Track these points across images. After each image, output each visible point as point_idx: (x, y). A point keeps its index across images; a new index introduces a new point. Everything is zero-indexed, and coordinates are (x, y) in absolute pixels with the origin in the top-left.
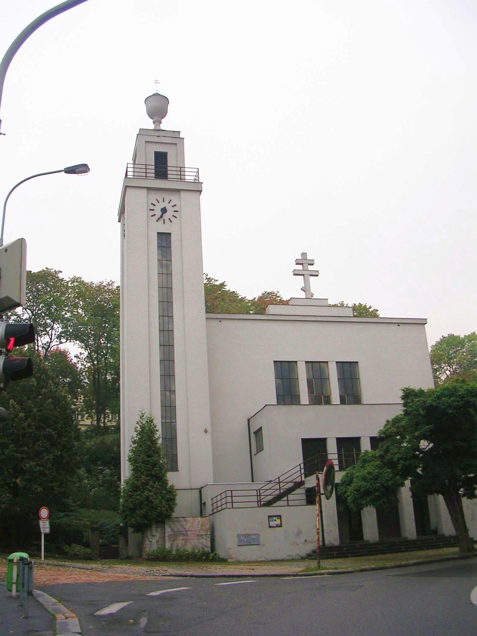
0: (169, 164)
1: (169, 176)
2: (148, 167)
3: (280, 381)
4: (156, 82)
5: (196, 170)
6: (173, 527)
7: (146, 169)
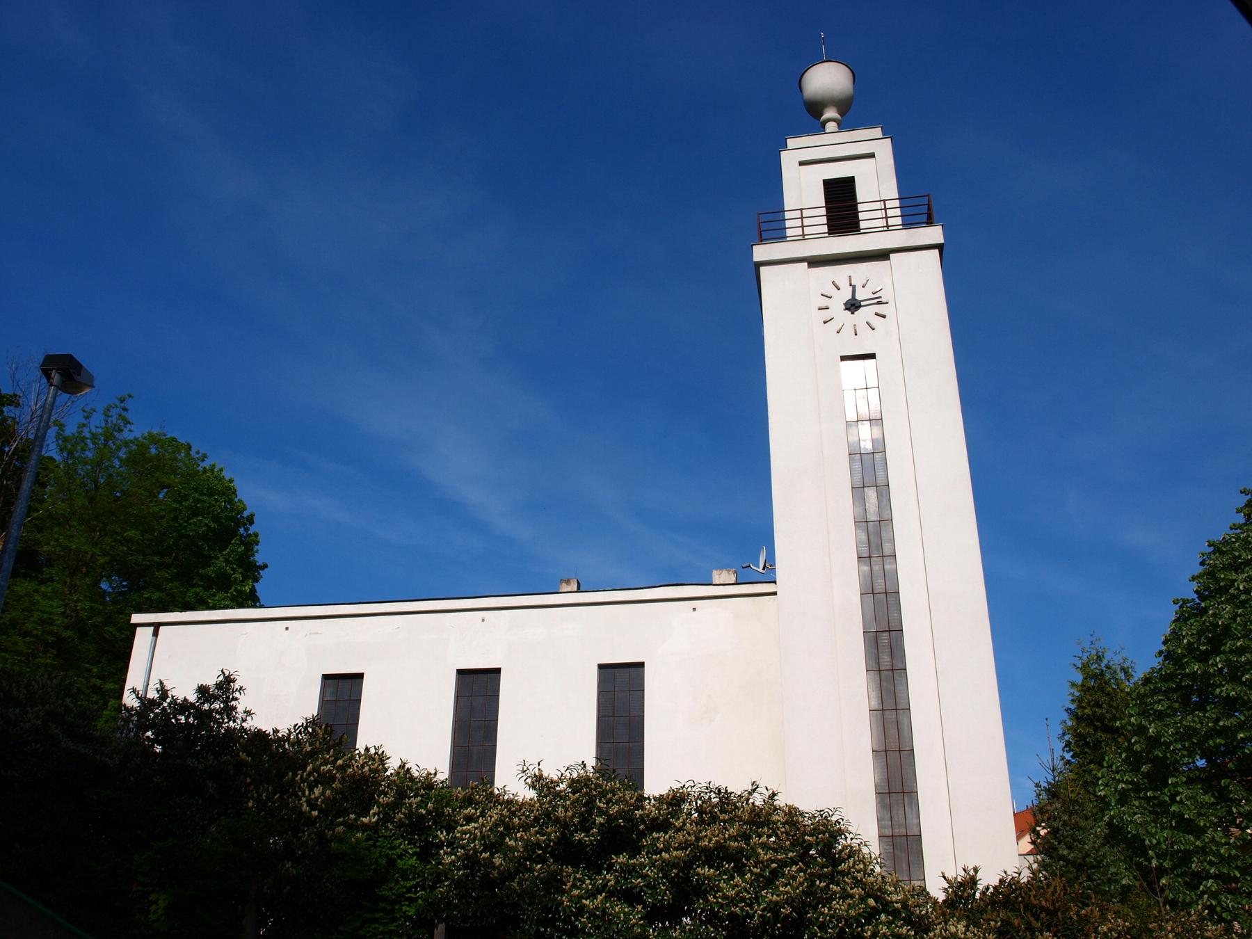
0: (860, 197)
1: (862, 225)
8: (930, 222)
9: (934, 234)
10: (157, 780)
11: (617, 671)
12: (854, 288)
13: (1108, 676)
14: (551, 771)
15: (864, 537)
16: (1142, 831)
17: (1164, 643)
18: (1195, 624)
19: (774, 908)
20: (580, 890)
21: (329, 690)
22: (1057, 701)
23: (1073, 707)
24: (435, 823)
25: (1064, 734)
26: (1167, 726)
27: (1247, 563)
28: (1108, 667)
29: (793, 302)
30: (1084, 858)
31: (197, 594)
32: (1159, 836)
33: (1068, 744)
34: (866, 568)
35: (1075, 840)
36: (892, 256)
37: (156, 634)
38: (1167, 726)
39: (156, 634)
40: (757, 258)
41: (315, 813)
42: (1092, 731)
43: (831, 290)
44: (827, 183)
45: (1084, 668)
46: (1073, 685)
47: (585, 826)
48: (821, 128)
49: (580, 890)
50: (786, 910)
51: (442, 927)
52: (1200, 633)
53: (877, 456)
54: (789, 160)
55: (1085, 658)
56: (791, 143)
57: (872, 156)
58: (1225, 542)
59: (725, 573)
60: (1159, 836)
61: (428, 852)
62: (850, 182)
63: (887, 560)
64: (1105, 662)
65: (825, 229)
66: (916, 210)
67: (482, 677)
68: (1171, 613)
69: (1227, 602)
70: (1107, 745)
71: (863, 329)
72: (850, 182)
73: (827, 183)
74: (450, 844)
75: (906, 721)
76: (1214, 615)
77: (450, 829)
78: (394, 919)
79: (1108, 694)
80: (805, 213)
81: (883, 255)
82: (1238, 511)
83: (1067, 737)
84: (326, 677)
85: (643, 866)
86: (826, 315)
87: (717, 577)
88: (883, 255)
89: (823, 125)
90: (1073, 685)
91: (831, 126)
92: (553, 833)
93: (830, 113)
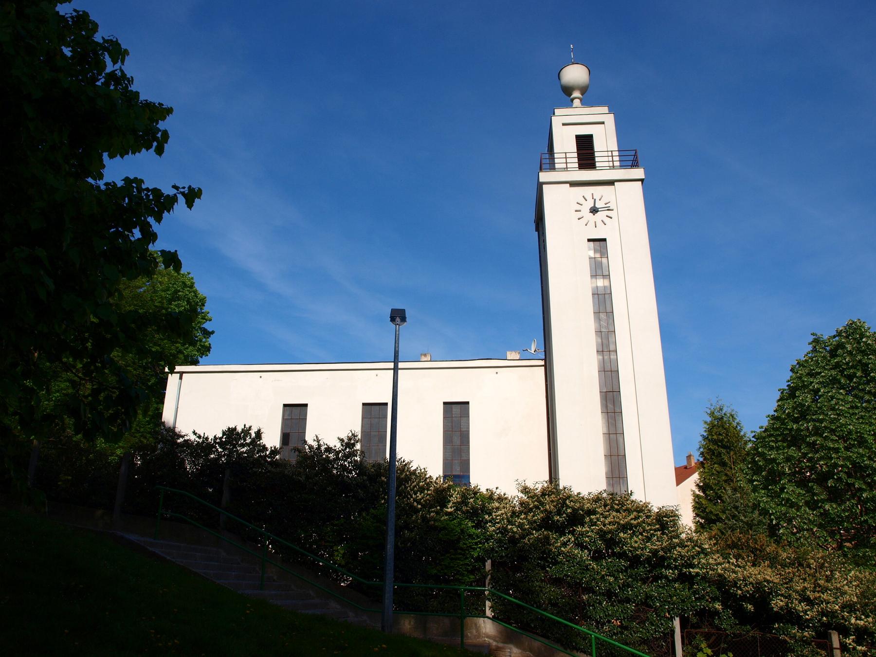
1: (597, 164)
8: (635, 165)
9: (639, 173)
10: (329, 489)
13: (725, 419)
14: (530, 484)
15: (600, 340)
18: (791, 402)
20: (564, 544)
21: (287, 413)
22: (697, 432)
23: (705, 434)
24: (482, 511)
29: (562, 204)
31: (177, 348)
32: (773, 508)
33: (702, 453)
34: (601, 357)
37: (181, 378)
39: (181, 378)
43: (582, 201)
45: (712, 414)
46: (706, 422)
47: (559, 513)
48: (569, 104)
49: (564, 544)
50: (661, 553)
51: (489, 561)
52: (794, 408)
54: (556, 122)
60: (773, 508)
63: (612, 353)
65: (577, 165)
66: (629, 159)
67: (377, 407)
68: (778, 395)
69: (808, 393)
71: (599, 224)
74: (490, 521)
75: (621, 440)
77: (490, 514)
78: (467, 558)
81: (611, 183)
82: (809, 344)
83: (702, 450)
84: (285, 405)
86: (579, 215)
87: (510, 355)
88: (611, 183)
89: (572, 100)
90: (706, 422)
91: (577, 102)
92: (540, 516)
93: (576, 94)
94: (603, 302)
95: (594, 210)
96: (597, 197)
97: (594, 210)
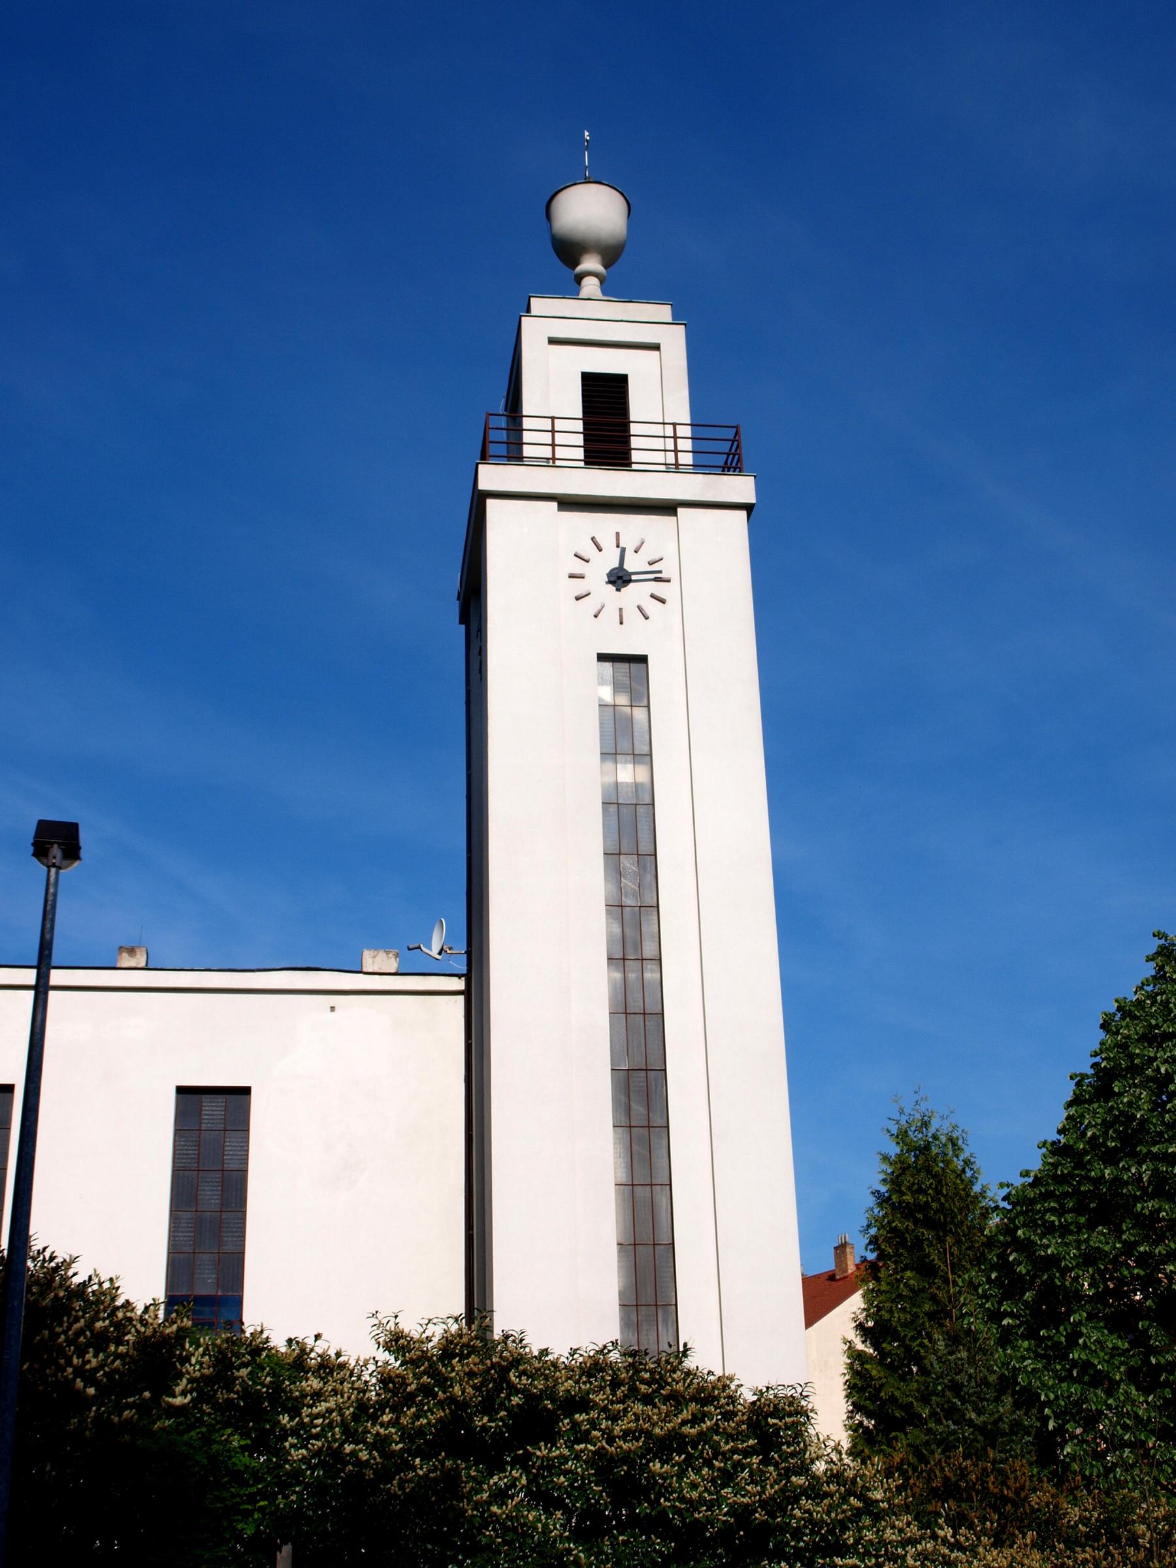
0: (634, 413)
1: (635, 456)
2: (546, 452)
3: (657, 1121)
4: (333, 1009)
5: (730, 433)
6: (634, 1340)
7: (553, 431)
8: (732, 465)
9: (742, 488)
11: (206, 1098)
12: (623, 551)
13: (935, 1150)
14: (411, 1326)
15: (617, 930)
16: (1036, 1383)
17: (1059, 1132)
19: (742, 1514)
20: (501, 1494)
22: (864, 1179)
23: (883, 1189)
25: (869, 1226)
26: (1066, 1245)
27: (1167, 1037)
28: (935, 1137)
29: (538, 562)
30: (995, 1423)
32: (1052, 1389)
35: (982, 1400)
36: (680, 510)
38: (1066, 1245)
40: (483, 485)
41: (91, 1391)
42: (911, 1226)
43: (589, 550)
44: (589, 380)
45: (901, 1136)
46: (885, 1158)
47: (488, 1407)
49: (501, 1494)
51: (287, 1549)
52: (1106, 1125)
53: (640, 810)
54: (534, 332)
55: (903, 1122)
56: (537, 305)
57: (656, 347)
58: (1139, 1004)
59: (382, 955)
60: (1052, 1389)
61: (267, 1441)
62: (618, 383)
63: (649, 966)
64: (932, 1130)
65: (580, 453)
66: (719, 449)
70: (931, 1245)
71: (632, 615)
72: (618, 383)
73: (589, 380)
74: (294, 1432)
75: (664, 1201)
76: (1130, 1103)
77: (295, 1412)
79: (934, 1176)
80: (559, 425)
82: (1149, 959)
83: (873, 1231)
85: (564, 1459)
86: (579, 587)
87: (373, 960)
88: (668, 508)
89: (579, 278)
90: (885, 1158)
91: (590, 286)
93: (591, 263)
94: (630, 833)
95: (619, 579)
96: (628, 543)
97: (619, 579)
